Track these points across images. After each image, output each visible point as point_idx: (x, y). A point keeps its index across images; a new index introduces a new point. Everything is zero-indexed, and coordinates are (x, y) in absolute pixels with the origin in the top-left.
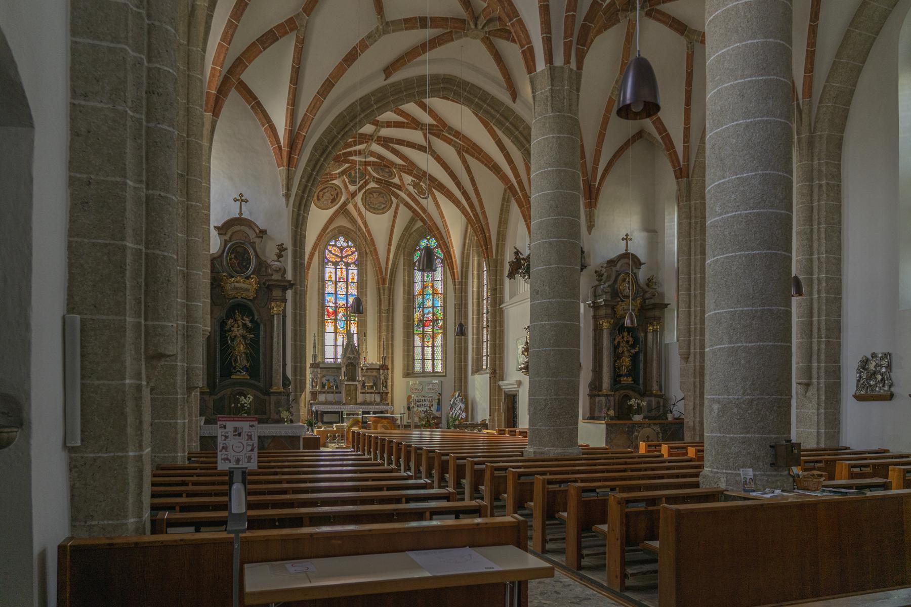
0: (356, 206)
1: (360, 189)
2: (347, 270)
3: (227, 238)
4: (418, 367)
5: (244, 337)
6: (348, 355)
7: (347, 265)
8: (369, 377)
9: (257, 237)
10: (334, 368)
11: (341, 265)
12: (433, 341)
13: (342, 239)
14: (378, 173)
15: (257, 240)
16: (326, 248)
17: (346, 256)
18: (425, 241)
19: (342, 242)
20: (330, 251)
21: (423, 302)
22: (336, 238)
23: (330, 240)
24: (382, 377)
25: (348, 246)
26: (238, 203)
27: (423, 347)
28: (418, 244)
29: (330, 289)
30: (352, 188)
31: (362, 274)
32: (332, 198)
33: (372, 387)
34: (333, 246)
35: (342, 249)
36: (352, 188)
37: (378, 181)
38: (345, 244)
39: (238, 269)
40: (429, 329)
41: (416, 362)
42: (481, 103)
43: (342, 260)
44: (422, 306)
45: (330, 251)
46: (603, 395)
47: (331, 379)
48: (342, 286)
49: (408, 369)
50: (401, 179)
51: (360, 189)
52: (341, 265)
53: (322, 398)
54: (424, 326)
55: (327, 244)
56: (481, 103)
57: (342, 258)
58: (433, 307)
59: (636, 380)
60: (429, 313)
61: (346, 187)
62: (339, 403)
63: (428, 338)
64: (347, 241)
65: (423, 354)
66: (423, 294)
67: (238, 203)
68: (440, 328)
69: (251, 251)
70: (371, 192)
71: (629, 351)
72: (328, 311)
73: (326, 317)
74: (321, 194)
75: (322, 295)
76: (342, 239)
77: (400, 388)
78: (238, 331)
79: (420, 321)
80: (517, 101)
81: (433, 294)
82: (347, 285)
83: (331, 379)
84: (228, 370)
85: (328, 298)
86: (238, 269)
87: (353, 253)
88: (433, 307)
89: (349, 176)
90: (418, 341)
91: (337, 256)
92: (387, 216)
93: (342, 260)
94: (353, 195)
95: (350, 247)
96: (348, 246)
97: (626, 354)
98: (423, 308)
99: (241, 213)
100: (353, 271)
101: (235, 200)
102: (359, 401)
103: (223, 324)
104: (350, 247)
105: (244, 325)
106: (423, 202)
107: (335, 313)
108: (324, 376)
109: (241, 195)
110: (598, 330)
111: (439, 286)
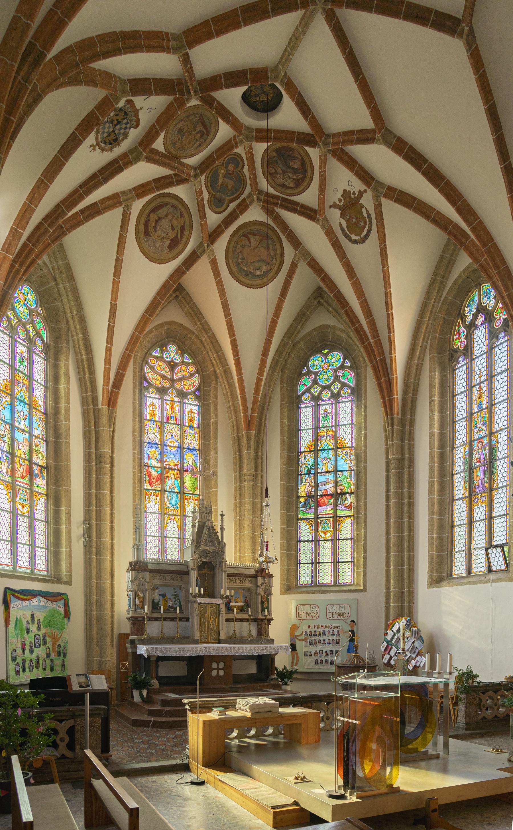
0: (214, 263)
1: (227, 222)
2: (182, 404)
4: (306, 576)
6: (203, 547)
7: (182, 395)
8: (236, 590)
10: (179, 572)
11: (172, 395)
12: (335, 529)
13: (172, 348)
17: (181, 379)
18: (320, 358)
19: (172, 352)
20: (152, 368)
21: (316, 464)
22: (163, 346)
23: (153, 347)
24: (261, 592)
25: (183, 363)
27: (316, 541)
28: (306, 364)
29: (152, 435)
30: (213, 218)
31: (204, 412)
32: (172, 235)
33: (242, 610)
34: (157, 358)
35: (172, 366)
36: (213, 218)
38: (178, 359)
40: (326, 510)
41: (456, 530)
43: (172, 386)
44: (314, 471)
45: (152, 368)
48: (172, 429)
49: (288, 580)
51: (227, 222)
52: (172, 395)
53: (153, 629)
54: (318, 505)
55: (147, 354)
57: (172, 381)
58: (336, 471)
60: (327, 482)
61: (202, 214)
62: (187, 639)
63: (326, 526)
64: (182, 351)
65: (316, 553)
66: (315, 450)
68: (350, 507)
70: (246, 232)
72: (149, 475)
73: (147, 486)
74: (153, 217)
75: (140, 444)
76: (172, 348)
77: (284, 610)
79: (309, 497)
81: (336, 449)
82: (182, 431)
85: (148, 451)
87: (192, 375)
88: (336, 471)
89: (212, 183)
90: (305, 531)
91: (164, 377)
93: (172, 386)
94: (213, 237)
95: (187, 364)
96: (183, 363)
98: (317, 474)
100: (192, 406)
102: (223, 636)
104: (187, 364)
106: (355, 252)
107: (162, 478)
108: (155, 588)
111: (346, 435)
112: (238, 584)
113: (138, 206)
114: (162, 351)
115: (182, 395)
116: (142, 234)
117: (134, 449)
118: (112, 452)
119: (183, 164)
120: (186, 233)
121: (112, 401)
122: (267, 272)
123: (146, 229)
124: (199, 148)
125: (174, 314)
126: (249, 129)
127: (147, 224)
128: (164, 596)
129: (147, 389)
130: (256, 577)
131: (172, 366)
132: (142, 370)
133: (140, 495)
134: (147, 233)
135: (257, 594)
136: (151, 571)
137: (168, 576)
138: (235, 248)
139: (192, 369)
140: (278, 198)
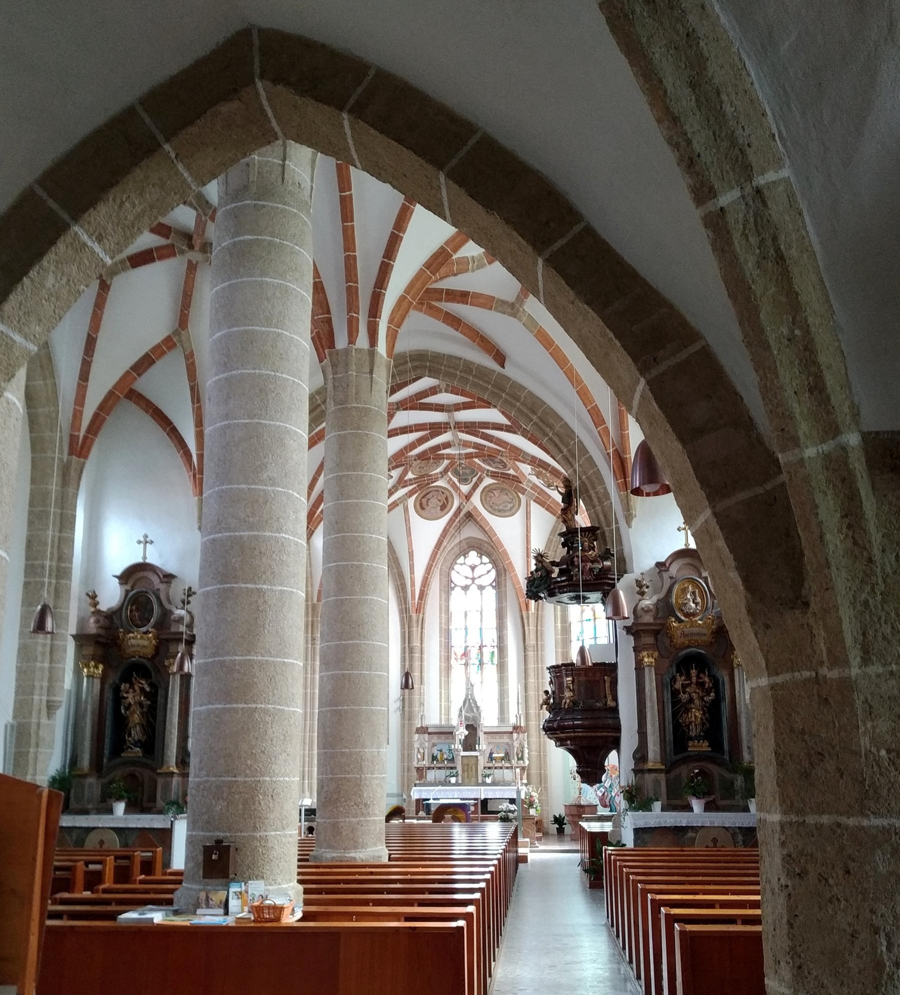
1: (474, 488)
3: (128, 587)
5: (141, 705)
7: (481, 588)
8: (498, 745)
9: (162, 582)
10: (447, 733)
11: (474, 588)
14: (491, 466)
15: (162, 587)
16: (451, 568)
19: (473, 554)
22: (465, 554)
23: (458, 557)
24: (516, 744)
25: (482, 563)
26: (142, 545)
30: (465, 488)
33: (502, 759)
37: (493, 475)
39: (139, 622)
42: (465, 376)
46: (650, 771)
47: (445, 750)
50: (517, 469)
55: (454, 562)
56: (465, 376)
57: (473, 579)
59: (716, 745)
67: (142, 545)
69: (153, 599)
70: (488, 490)
71: (702, 698)
73: (453, 662)
78: (131, 698)
80: (506, 364)
83: (445, 750)
84: (119, 746)
86: (139, 622)
89: (456, 473)
92: (517, 519)
94: (468, 497)
97: (697, 702)
99: (145, 557)
100: (490, 594)
101: (139, 542)
103: (117, 690)
105: (142, 690)
108: (434, 745)
109: (146, 536)
110: (639, 668)
112: (497, 739)
113: (411, 501)
114: (465, 558)
115: (481, 588)
116: (420, 510)
117: (440, 637)
118: (421, 644)
119: (431, 476)
120: (450, 500)
121: (420, 609)
122: (511, 508)
123: (421, 507)
124: (438, 466)
125: (470, 532)
126: (441, 473)
127: (421, 504)
128: (441, 751)
129: (453, 589)
130: (512, 733)
131: (473, 568)
132: (449, 575)
133: (447, 670)
134: (422, 508)
135: (514, 747)
136: (429, 734)
137: (443, 736)
138: (486, 499)
139: (490, 566)
140: (498, 473)
